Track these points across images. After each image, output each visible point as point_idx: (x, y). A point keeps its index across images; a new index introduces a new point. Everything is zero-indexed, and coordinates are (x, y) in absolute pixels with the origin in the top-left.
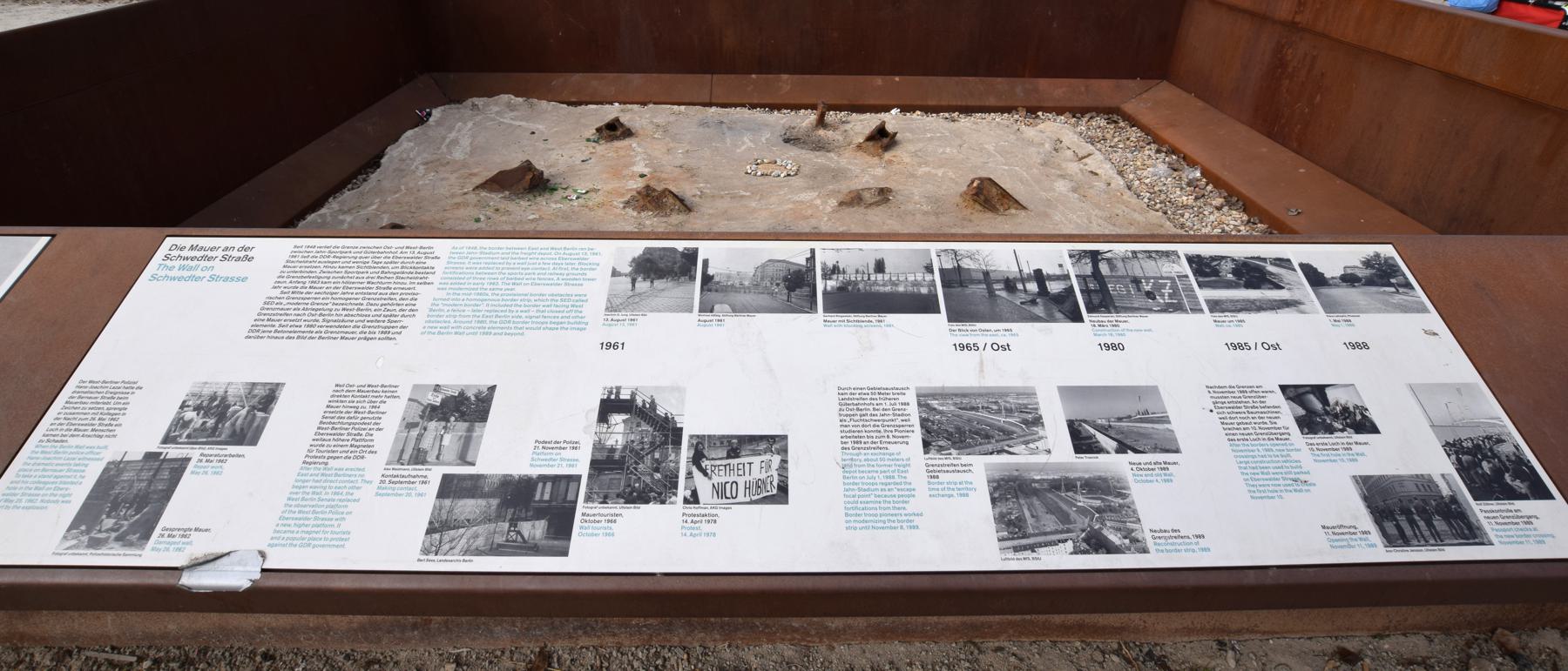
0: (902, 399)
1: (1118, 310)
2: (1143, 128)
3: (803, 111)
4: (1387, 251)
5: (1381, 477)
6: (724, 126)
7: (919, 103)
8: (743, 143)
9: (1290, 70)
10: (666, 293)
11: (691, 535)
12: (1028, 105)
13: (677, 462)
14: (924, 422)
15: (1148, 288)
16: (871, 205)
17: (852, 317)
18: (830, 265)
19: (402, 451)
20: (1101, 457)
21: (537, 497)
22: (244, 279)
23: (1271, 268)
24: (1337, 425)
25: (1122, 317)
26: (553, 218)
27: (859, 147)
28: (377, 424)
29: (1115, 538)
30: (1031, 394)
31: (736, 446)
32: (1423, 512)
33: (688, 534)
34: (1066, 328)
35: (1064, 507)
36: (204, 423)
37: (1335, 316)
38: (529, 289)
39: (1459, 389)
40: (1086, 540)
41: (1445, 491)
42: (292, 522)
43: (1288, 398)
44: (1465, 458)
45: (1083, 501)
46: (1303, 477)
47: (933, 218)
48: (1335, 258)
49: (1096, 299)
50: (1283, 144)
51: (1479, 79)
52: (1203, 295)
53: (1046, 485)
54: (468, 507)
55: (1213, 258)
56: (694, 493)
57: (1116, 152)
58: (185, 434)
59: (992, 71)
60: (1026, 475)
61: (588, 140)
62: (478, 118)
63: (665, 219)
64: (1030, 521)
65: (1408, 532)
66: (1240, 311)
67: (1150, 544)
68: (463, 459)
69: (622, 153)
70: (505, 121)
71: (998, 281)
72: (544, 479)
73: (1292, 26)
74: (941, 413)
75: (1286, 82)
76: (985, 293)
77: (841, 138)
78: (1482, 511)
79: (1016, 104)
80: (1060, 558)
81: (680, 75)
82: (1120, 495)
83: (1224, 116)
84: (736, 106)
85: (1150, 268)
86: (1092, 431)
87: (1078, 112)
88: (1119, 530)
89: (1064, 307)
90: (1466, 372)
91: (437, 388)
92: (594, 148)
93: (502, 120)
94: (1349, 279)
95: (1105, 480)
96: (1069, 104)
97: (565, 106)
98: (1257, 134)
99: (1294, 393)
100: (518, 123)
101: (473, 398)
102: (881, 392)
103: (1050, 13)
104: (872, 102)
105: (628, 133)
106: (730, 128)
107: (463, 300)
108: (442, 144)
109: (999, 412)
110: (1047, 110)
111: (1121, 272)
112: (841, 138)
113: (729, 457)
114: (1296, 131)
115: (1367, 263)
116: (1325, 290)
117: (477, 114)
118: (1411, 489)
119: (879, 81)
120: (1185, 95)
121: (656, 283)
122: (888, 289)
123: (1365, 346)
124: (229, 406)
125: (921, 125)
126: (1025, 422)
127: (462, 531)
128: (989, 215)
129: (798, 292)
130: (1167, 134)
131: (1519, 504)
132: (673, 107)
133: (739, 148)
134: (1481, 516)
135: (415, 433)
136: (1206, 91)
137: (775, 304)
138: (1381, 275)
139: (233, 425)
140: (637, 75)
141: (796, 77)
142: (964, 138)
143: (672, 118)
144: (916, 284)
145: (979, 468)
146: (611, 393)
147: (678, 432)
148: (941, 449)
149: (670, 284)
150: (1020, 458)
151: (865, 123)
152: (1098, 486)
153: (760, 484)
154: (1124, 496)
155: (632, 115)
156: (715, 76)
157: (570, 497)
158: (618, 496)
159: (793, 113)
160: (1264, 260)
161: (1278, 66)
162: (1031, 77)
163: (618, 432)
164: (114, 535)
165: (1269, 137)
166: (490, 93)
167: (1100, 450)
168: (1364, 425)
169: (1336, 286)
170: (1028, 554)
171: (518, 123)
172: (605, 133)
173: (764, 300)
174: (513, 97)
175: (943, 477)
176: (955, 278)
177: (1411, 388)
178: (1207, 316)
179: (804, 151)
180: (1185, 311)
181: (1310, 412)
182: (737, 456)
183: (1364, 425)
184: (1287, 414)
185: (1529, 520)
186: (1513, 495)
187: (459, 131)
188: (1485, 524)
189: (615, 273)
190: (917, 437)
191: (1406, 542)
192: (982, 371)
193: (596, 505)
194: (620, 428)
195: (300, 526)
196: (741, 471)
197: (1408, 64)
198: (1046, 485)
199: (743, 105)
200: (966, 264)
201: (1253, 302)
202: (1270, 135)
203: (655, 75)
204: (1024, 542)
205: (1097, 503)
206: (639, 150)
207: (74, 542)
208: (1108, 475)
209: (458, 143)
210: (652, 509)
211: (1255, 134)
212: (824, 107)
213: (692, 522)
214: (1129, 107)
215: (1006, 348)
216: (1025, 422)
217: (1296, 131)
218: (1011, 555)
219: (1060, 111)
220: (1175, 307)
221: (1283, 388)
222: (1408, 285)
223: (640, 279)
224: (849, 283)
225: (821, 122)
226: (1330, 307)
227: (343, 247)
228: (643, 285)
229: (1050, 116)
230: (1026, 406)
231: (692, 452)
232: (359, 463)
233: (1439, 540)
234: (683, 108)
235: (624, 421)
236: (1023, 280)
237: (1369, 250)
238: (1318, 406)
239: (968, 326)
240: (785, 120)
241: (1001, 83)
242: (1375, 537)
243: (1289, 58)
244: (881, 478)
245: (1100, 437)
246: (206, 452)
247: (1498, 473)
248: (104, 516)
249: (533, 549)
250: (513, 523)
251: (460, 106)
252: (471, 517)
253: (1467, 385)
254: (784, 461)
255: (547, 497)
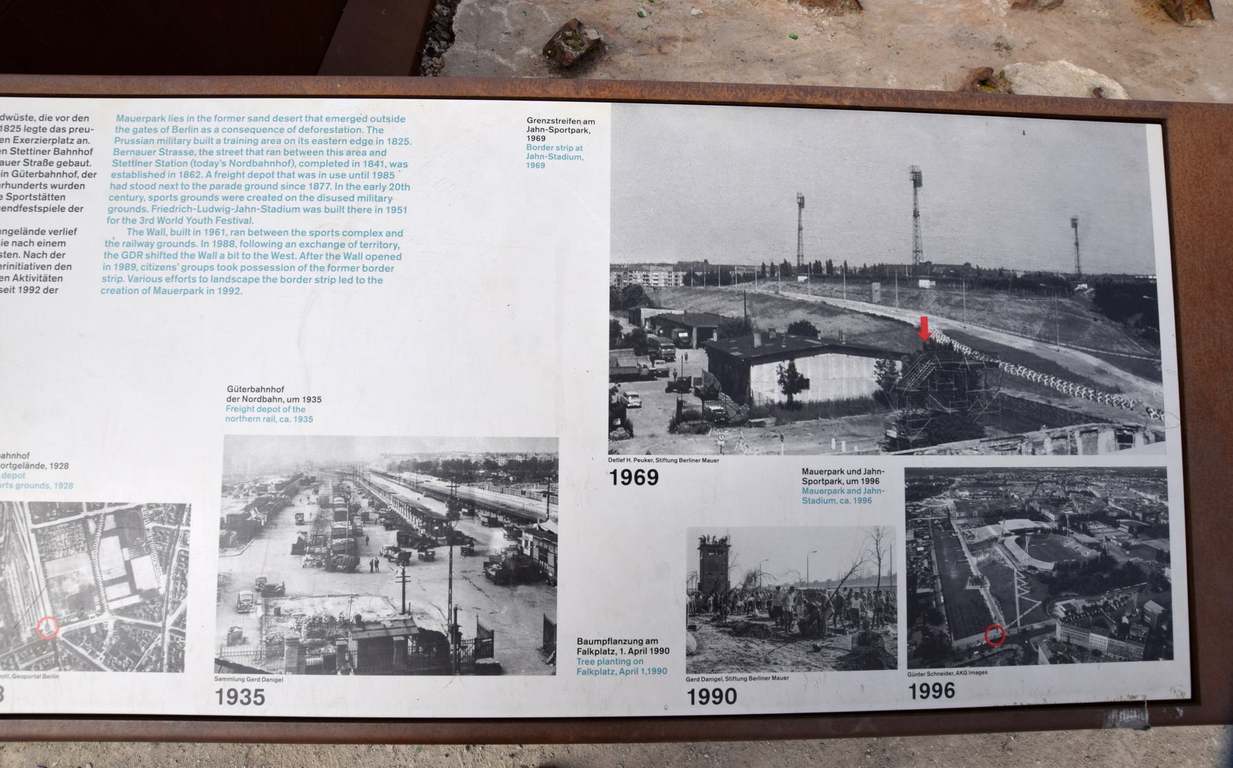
11: (622, 671)
16: (1045, 7)
26: (718, 13)
28: (58, 256)
33: (617, 671)
47: (1113, 29)
63: (840, 19)
107: (217, 130)
128: (1172, 26)
213: (631, 651)
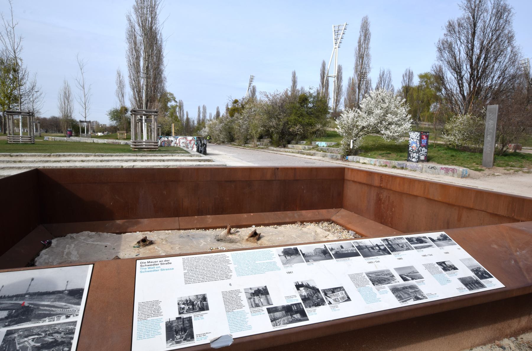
0: (363, 275)
1: (397, 251)
2: (340, 225)
3: (218, 229)
4: (443, 233)
5: (463, 278)
6: (190, 237)
7: (262, 223)
8: (202, 243)
9: (383, 201)
10: (295, 259)
12: (300, 220)
13: (322, 296)
14: (370, 279)
15: (401, 246)
17: (342, 259)
18: (330, 248)
19: (252, 305)
20: (409, 281)
21: (294, 309)
22: (173, 269)
23: (423, 239)
24: (450, 269)
25: (399, 252)
27: (247, 240)
29: (420, 297)
30: (389, 271)
31: (333, 290)
32: (473, 283)
34: (388, 256)
35: (408, 292)
36: (189, 307)
37: (440, 247)
38: (259, 262)
39: (469, 259)
40: (415, 298)
41: (475, 279)
42: (234, 326)
43: (439, 265)
44: (475, 272)
45: (410, 291)
46: (449, 280)
48: (435, 235)
49: (392, 249)
50: (386, 225)
51: (436, 199)
52: (413, 246)
53: (402, 289)
54: (277, 314)
55: (411, 238)
56: (330, 302)
57: (335, 234)
58: (185, 311)
59: (286, 209)
60: (397, 287)
61: (134, 247)
62: (76, 242)
64: (402, 296)
65: (472, 287)
66: (421, 248)
67: (427, 297)
68: (269, 303)
69: (152, 251)
70: (89, 243)
71: (370, 248)
72: (293, 305)
73: (380, 188)
74: (373, 277)
75: (383, 205)
76: (368, 250)
77: (239, 238)
78: (483, 281)
79: (296, 220)
80: (411, 302)
81: (165, 218)
82: (417, 288)
83: (365, 218)
84: (190, 229)
85: (399, 241)
86: (405, 276)
87: (317, 221)
88: (420, 295)
89: (385, 252)
90: (468, 256)
91: (251, 289)
92: (138, 250)
93: (87, 242)
94: (439, 240)
95: (412, 286)
96: (314, 219)
97: (115, 234)
98: (377, 223)
99: (440, 264)
100: (96, 243)
101: (262, 290)
102: (358, 274)
103: (303, 188)
104: (244, 224)
105: (151, 243)
106: (193, 238)
108: (63, 255)
109: (384, 275)
110: (307, 222)
111: (394, 243)
112: (239, 238)
113: (333, 293)
114: (389, 221)
115: (441, 236)
116: (435, 242)
117: (75, 241)
118: (469, 279)
119: (245, 215)
120: (350, 213)
121: (291, 257)
122: (346, 252)
123: (448, 253)
124: (193, 302)
125: (266, 230)
126: (391, 276)
127: (280, 320)
129: (326, 255)
130: (349, 226)
131: (488, 279)
132: (165, 231)
133: (201, 244)
134: (483, 282)
135: (252, 300)
136: (356, 210)
137: (323, 258)
138: (445, 238)
139: (198, 306)
140: (146, 220)
141: (213, 216)
142: (284, 233)
143: (167, 236)
144: (352, 250)
145: (387, 287)
146: (296, 283)
147: (318, 290)
148: (377, 284)
149: (295, 257)
150: (393, 284)
151: (246, 232)
152: (412, 287)
153: (343, 298)
154: (418, 288)
155: (151, 236)
156: (180, 218)
157: (301, 308)
158: (313, 305)
159: (214, 230)
160: (421, 237)
161: (379, 201)
162: (299, 210)
163: (304, 292)
164: (182, 339)
165: (382, 224)
166: (78, 231)
167: (408, 280)
168: (455, 269)
169: (437, 241)
170: (405, 302)
171: (96, 243)
172: (141, 244)
173: (319, 258)
174: (89, 232)
175: (381, 290)
176: (360, 248)
177: (460, 260)
178: (415, 250)
179: (227, 244)
180: (410, 250)
181: (444, 267)
182: (334, 293)
183: (455, 269)
184: (440, 268)
185: (491, 282)
186: (486, 278)
187: (69, 248)
188: (484, 284)
189: (279, 256)
190: (370, 283)
191: (473, 289)
192: (376, 267)
193: (309, 308)
194: (304, 291)
195: (236, 327)
196: (337, 295)
197: (416, 196)
198: (402, 289)
199: (194, 229)
200: (360, 244)
201: (423, 246)
202: (382, 223)
203: (153, 219)
204: (403, 300)
205: (413, 290)
206: (159, 249)
207: (171, 343)
208: (413, 285)
209: (71, 254)
210: (322, 307)
211: (377, 223)
212: (230, 226)
214: (334, 218)
215: (379, 262)
216: (391, 276)
217: (389, 221)
218: (402, 303)
219: (311, 222)
220: (408, 249)
221: (437, 263)
222: (450, 240)
223: (287, 256)
224: (337, 252)
225: (229, 233)
226: (438, 246)
227: (211, 256)
228: (288, 258)
229: (309, 224)
230: (389, 273)
231: (324, 294)
232: (241, 310)
233: (478, 288)
234: (170, 231)
235: (304, 289)
236: (375, 247)
237: (440, 233)
238: (445, 266)
239: (368, 258)
240: (213, 233)
241: (289, 213)
242: (467, 289)
243: (382, 197)
244: (368, 292)
245: (407, 277)
246: (195, 314)
247: (482, 274)
248: (175, 336)
249: (300, 320)
250: (291, 315)
251: (65, 238)
252: (280, 316)
253: (470, 258)
254: (345, 292)
255: (296, 309)
